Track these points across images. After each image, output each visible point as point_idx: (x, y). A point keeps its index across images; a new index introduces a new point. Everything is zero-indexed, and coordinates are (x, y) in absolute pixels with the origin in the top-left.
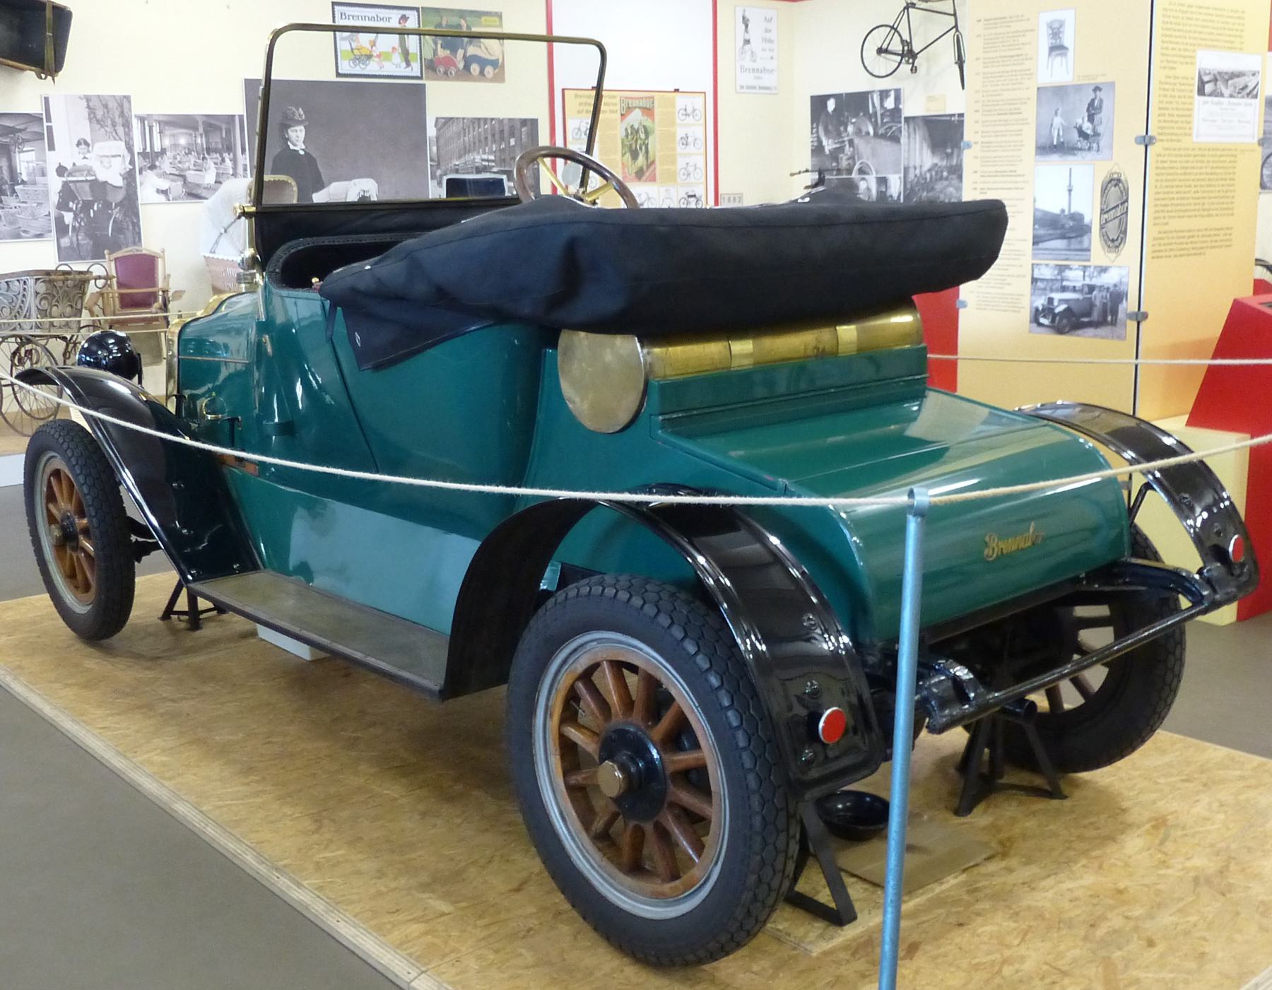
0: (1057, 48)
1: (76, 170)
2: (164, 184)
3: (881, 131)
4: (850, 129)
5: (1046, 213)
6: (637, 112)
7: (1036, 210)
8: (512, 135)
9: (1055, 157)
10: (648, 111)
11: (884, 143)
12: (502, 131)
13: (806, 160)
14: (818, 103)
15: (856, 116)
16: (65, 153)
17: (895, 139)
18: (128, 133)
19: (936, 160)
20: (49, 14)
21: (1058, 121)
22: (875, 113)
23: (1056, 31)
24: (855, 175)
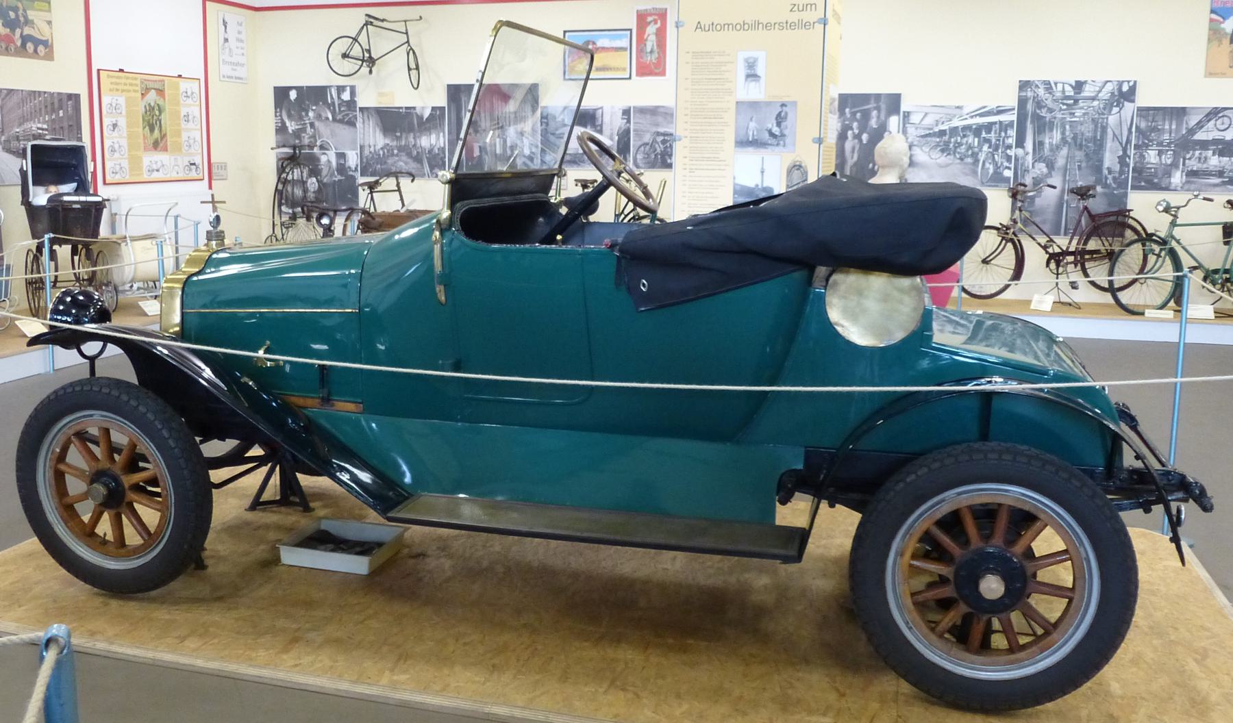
0: (752, 76)
3: (339, 117)
4: (311, 114)
5: (743, 187)
6: (152, 94)
7: (735, 185)
8: (61, 108)
9: (750, 149)
10: (160, 92)
11: (341, 126)
12: (53, 104)
13: (271, 138)
14: (281, 94)
15: (316, 104)
17: (352, 123)
19: (387, 141)
21: (752, 125)
22: (333, 103)
23: (751, 65)
24: (316, 150)
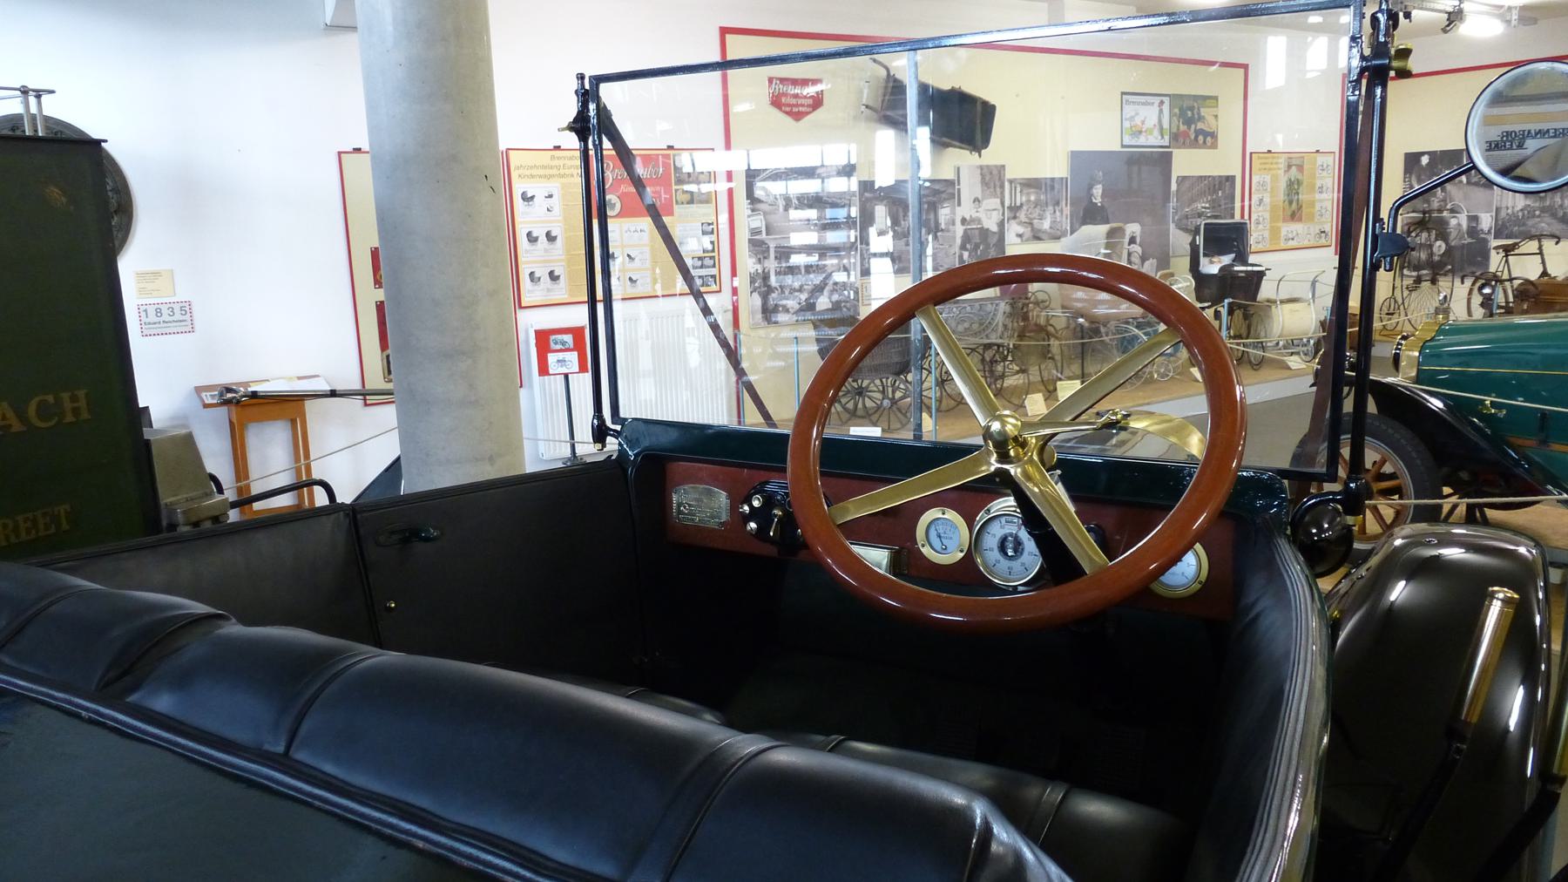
1: (973, 220)
2: (1021, 230)
10: (1300, 168)
11: (1476, 189)
16: (966, 210)
18: (1002, 193)
20: (979, 108)
